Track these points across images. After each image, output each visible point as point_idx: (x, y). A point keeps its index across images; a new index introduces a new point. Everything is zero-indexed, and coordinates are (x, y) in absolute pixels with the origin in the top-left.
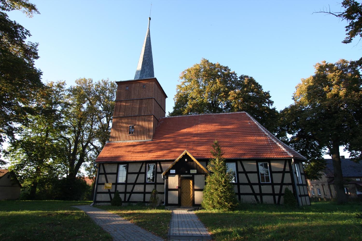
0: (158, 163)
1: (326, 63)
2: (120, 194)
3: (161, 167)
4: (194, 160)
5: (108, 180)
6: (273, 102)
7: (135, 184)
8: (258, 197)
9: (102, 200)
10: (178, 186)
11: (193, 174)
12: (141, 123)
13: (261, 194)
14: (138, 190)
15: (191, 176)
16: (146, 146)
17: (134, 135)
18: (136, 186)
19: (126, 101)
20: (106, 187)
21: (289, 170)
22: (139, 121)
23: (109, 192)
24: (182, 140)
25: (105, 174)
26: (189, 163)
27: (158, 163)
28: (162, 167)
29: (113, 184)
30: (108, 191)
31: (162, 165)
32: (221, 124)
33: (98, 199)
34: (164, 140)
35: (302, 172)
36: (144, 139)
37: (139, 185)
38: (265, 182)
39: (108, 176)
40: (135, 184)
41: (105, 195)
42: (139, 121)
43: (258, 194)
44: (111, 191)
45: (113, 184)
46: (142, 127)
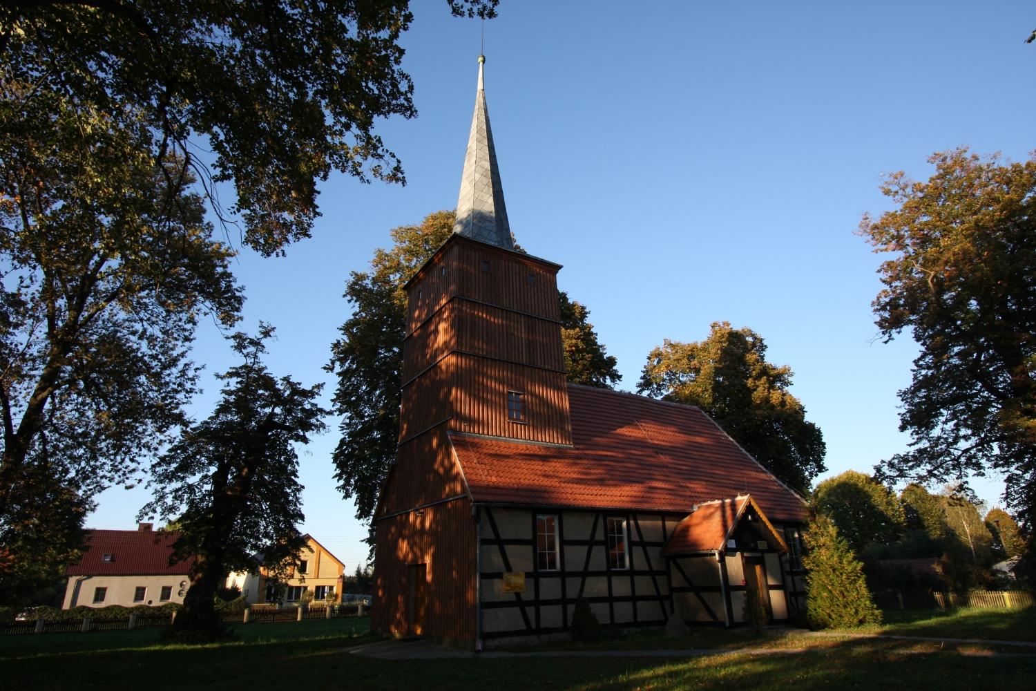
0: (631, 517)
1: (730, 327)
2: (592, 605)
3: (637, 524)
4: (764, 519)
5: (511, 560)
6: (619, 377)
7: (585, 574)
8: (531, 611)
9: (502, 629)
10: (743, 578)
11: (763, 551)
12: (540, 390)
13: (538, 603)
14: (595, 591)
15: (759, 555)
16: (576, 464)
17: (525, 425)
18: (590, 581)
19: (488, 308)
20: (508, 584)
21: (602, 538)
22: (533, 381)
23: (519, 602)
24: (641, 457)
25: (501, 543)
26: (754, 524)
27: (631, 517)
28: (641, 529)
29: (528, 575)
30: (514, 598)
31: (640, 522)
32: (684, 429)
33: (489, 627)
34: (605, 453)
35: (310, 543)
36: (552, 439)
37: (595, 578)
38: (548, 570)
39: (508, 548)
40: (585, 574)
41: (507, 610)
42: (531, 382)
43: (529, 603)
44: (525, 597)
45: (528, 575)
46: (543, 401)
